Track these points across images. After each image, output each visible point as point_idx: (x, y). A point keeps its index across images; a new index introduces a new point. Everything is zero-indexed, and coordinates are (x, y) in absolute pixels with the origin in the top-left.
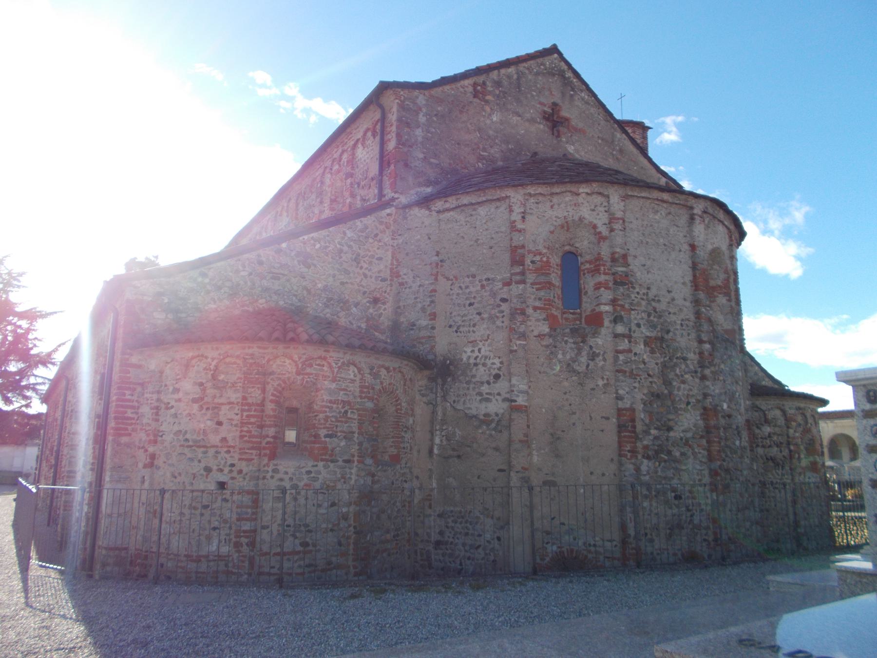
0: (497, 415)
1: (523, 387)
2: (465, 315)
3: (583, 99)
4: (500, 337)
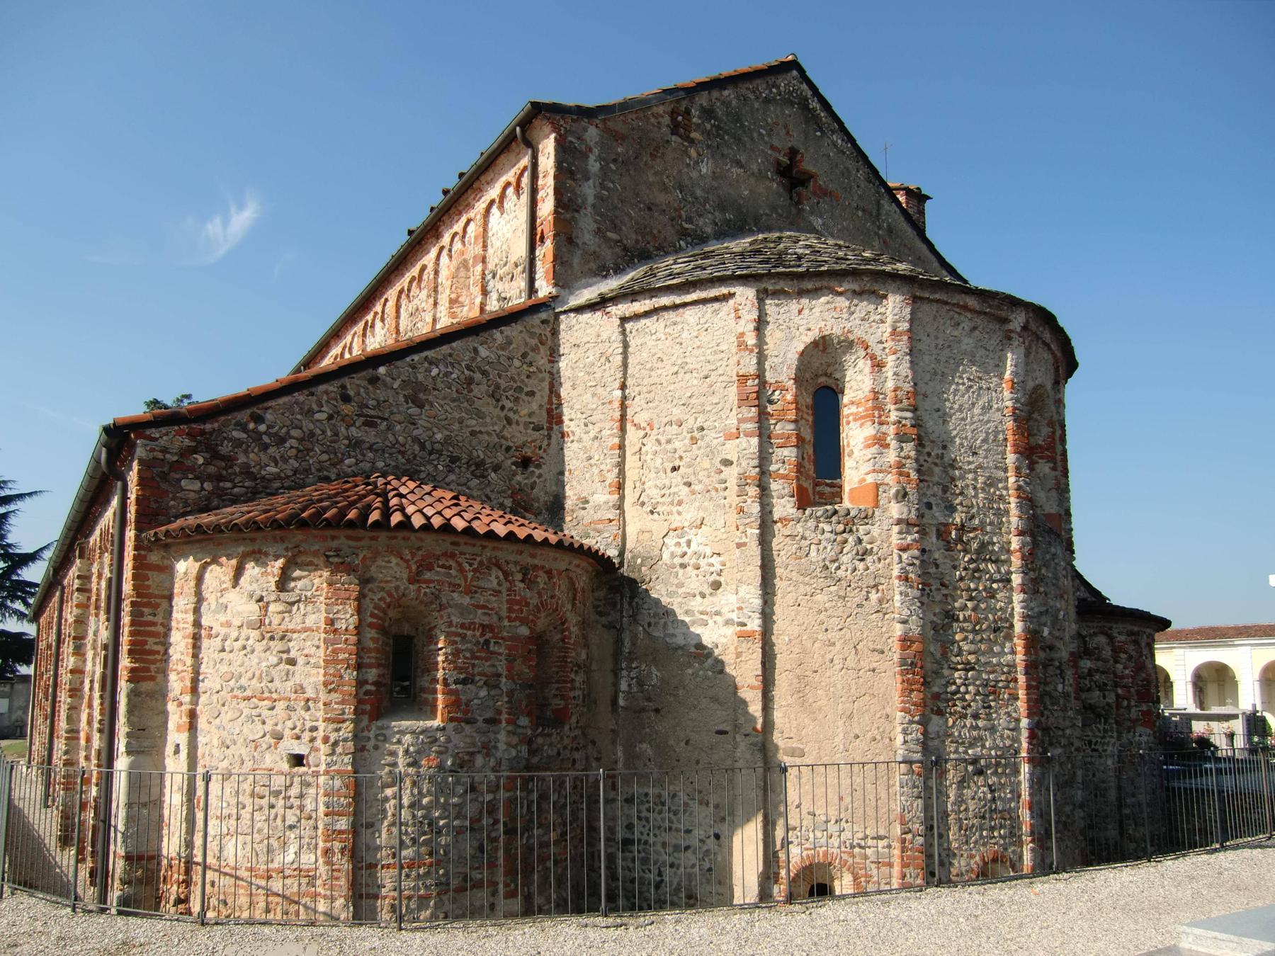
3: (835, 144)
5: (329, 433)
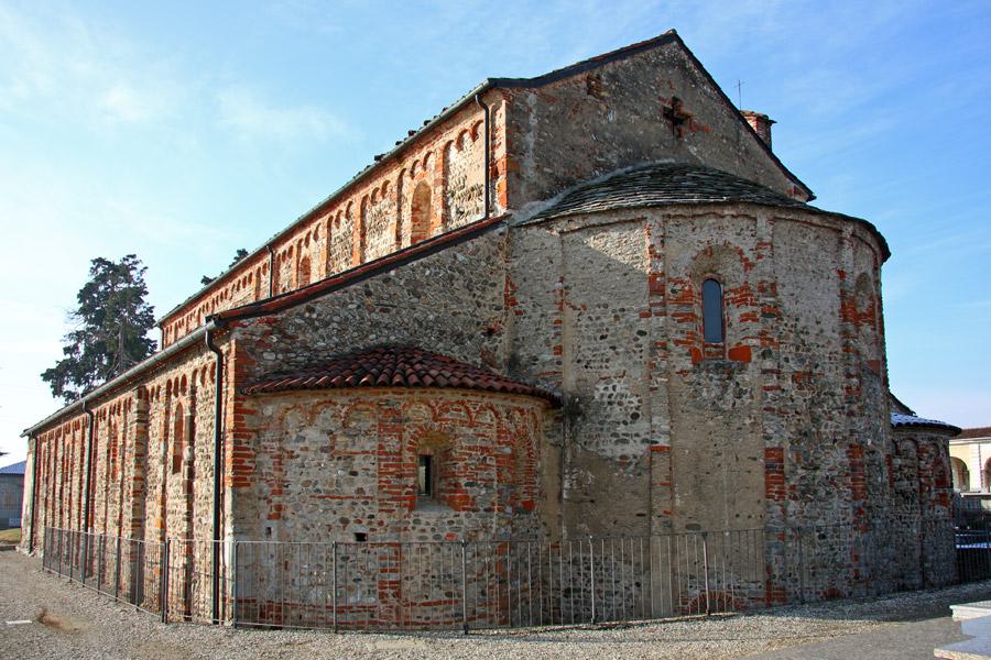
0: (635, 457)
1: (666, 427)
2: (595, 349)
4: (638, 373)
5: (358, 318)
